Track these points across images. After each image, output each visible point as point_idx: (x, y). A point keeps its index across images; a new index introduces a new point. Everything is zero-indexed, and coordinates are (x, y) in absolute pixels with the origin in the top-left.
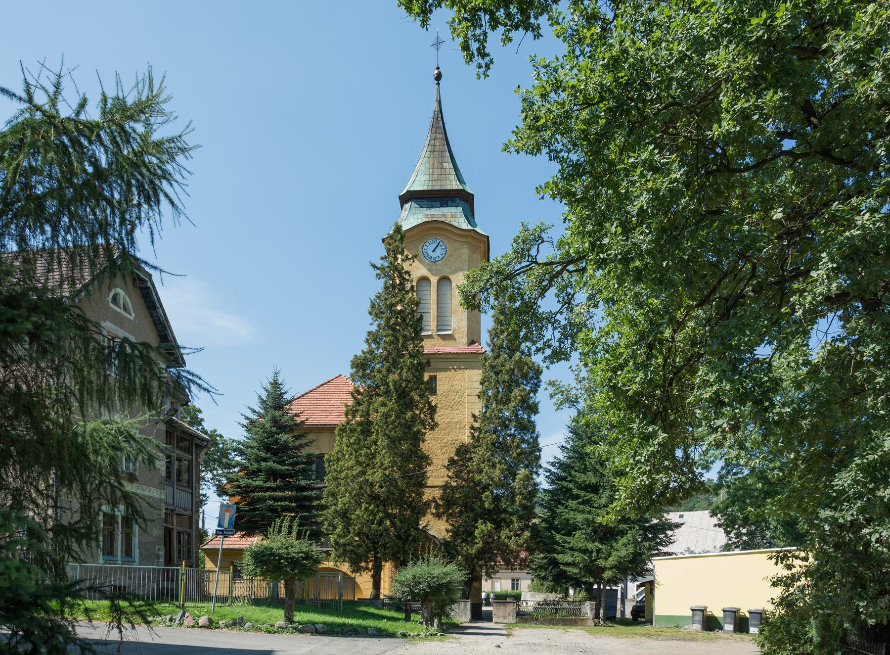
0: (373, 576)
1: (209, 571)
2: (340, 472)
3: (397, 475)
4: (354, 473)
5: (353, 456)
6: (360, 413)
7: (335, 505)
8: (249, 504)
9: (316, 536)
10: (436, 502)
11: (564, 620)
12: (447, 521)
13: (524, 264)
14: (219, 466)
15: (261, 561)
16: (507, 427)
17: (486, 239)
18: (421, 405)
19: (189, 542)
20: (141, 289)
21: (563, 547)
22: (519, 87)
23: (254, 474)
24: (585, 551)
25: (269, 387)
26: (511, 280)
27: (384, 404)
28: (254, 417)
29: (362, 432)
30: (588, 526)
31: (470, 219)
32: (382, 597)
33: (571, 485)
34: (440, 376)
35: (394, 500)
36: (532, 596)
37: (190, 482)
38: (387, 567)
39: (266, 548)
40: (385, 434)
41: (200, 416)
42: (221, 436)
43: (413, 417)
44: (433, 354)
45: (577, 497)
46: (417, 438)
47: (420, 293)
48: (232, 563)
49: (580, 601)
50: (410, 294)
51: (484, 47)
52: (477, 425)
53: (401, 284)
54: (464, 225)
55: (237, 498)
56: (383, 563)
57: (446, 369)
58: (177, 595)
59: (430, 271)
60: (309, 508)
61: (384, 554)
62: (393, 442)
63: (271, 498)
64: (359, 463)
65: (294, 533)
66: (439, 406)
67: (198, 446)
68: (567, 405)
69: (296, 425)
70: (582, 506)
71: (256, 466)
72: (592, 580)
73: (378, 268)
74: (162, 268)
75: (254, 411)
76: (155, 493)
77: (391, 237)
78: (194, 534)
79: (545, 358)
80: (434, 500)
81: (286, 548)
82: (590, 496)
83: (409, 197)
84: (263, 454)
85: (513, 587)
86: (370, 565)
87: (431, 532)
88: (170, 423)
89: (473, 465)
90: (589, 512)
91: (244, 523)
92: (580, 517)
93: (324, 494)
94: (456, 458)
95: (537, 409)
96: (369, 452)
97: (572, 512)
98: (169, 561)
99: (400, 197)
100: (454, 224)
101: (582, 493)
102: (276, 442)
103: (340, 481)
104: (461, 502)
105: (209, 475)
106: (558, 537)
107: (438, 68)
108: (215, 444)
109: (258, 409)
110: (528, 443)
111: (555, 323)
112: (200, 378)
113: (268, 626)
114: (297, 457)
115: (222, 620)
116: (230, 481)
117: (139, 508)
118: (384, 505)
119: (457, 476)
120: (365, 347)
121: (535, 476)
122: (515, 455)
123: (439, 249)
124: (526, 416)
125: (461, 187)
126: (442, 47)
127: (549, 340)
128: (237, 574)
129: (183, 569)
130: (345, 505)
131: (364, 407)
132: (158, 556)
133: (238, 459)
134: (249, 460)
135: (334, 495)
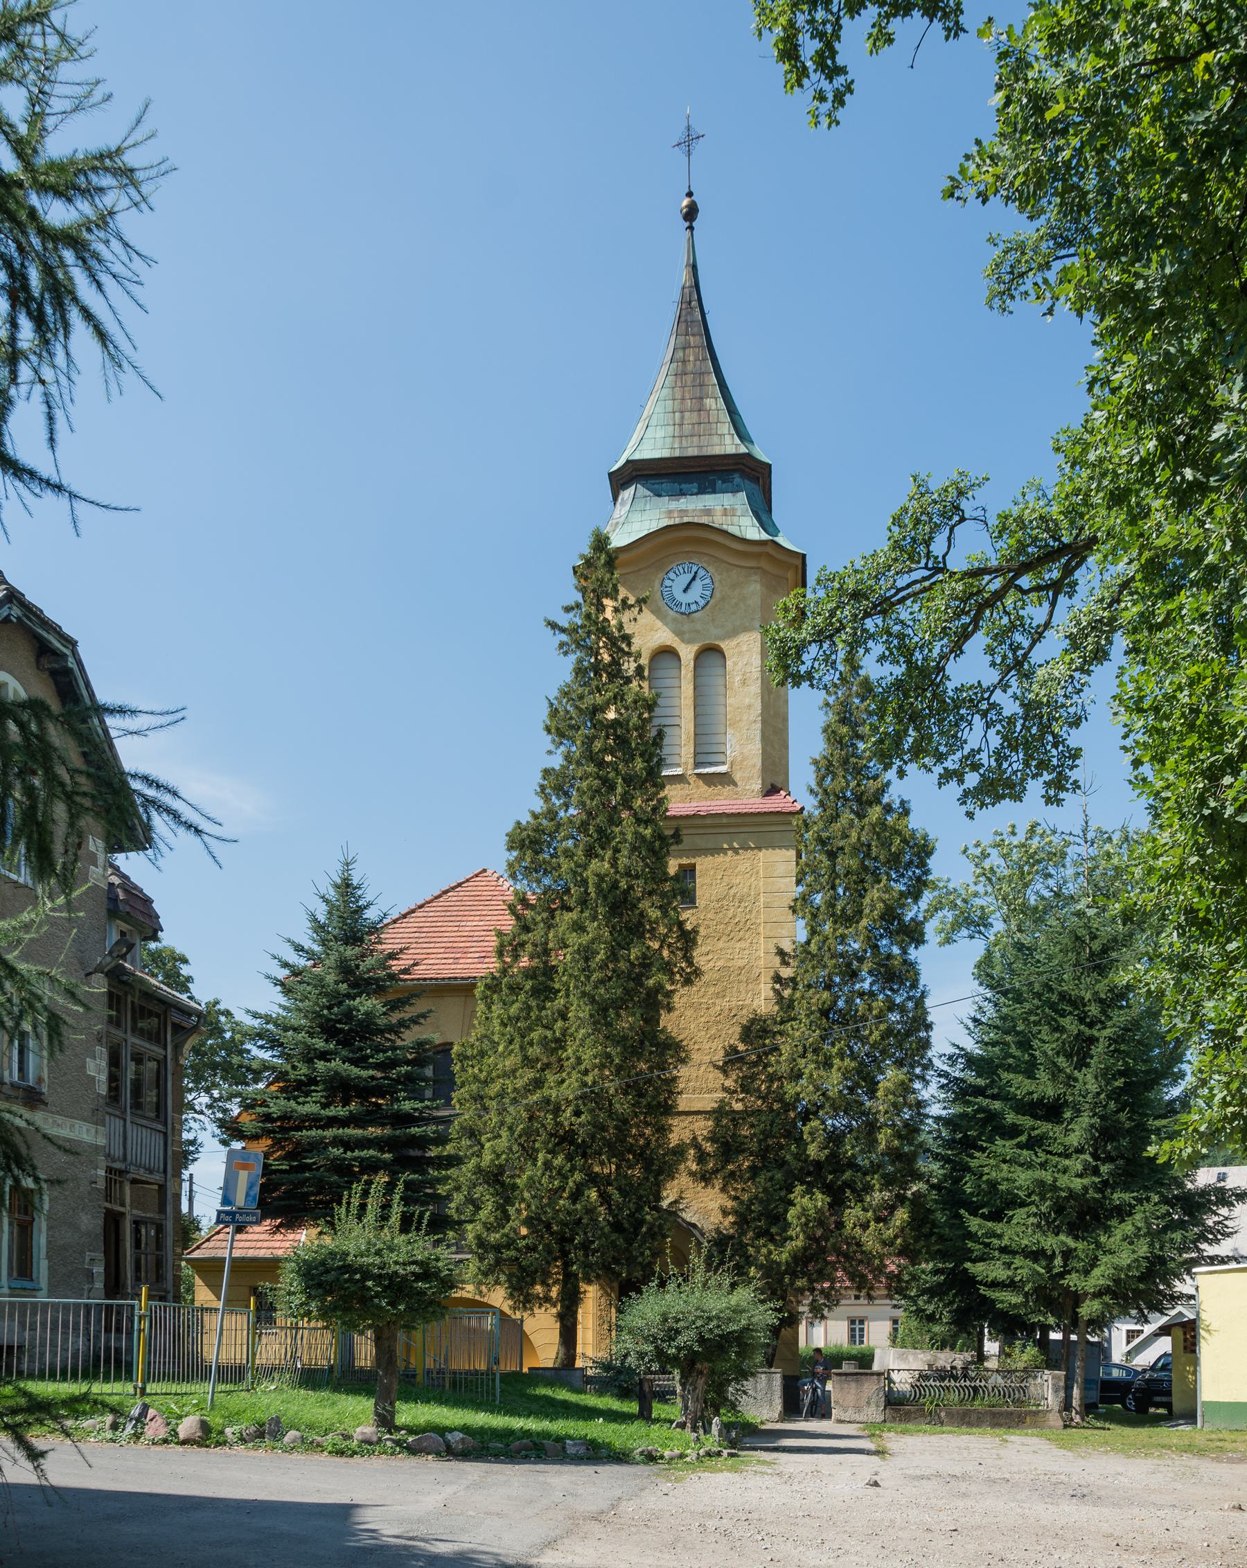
0: (561, 1317)
1: (203, 1310)
2: (486, 1083)
3: (611, 1087)
4: (519, 1083)
5: (516, 1046)
6: (529, 947)
7: (479, 1155)
8: (289, 1156)
9: (440, 1224)
10: (697, 1147)
11: (994, 1415)
12: (723, 1190)
13: (917, 575)
14: (224, 1079)
15: (320, 1285)
16: (854, 975)
17: (799, 562)
18: (663, 930)
19: (159, 1243)
20: (53, 674)
21: (987, 1245)
22: (990, 19)
23: (300, 1088)
24: (1036, 1255)
25: (332, 894)
26: (884, 612)
27: (578, 927)
28: (302, 962)
29: (535, 992)
30: (1043, 1199)
31: (764, 518)
32: (579, 1363)
33: (997, 1105)
34: (704, 864)
35: (608, 1144)
36: (901, 1357)
37: (160, 1108)
38: (592, 1295)
39: (332, 1254)
40: (584, 994)
41: (185, 970)
42: (228, 1013)
43: (644, 956)
44: (688, 817)
45: (1013, 1132)
46: (655, 1003)
47: (657, 683)
48: (254, 1291)
49: (1025, 1370)
50: (634, 684)
51: (833, 53)
52: (786, 973)
53: (615, 663)
54: (753, 532)
55: (266, 1143)
56: (583, 1286)
57: (717, 850)
58: (129, 1365)
59: (679, 633)
60: (420, 1164)
61: (586, 1266)
62: (602, 1012)
63: (338, 1141)
64: (528, 1062)
65: (395, 1219)
66: (702, 931)
67: (177, 1028)
68: (964, 932)
69: (392, 977)
70: (1025, 1152)
71: (304, 1069)
72: (1051, 1320)
73: (563, 630)
74: (74, 488)
75: (299, 948)
76: (83, 1133)
77: (589, 563)
78: (169, 1226)
79: (966, 793)
80: (695, 1143)
81: (378, 1253)
82: (1044, 1127)
83: (623, 478)
84: (319, 1044)
85: (852, 1337)
86: (554, 1292)
87: (688, 1216)
88: (117, 976)
89: (780, 1063)
90: (1043, 1165)
91: (279, 1198)
92: (1024, 1178)
93: (454, 1130)
94: (741, 1047)
95: (922, 934)
96: (549, 1034)
97: (1005, 1167)
98: (114, 1286)
99: (610, 475)
100: (732, 530)
101: (1026, 1121)
102: (348, 1015)
103: (488, 1102)
104: (754, 1146)
105: (204, 1099)
106: (974, 1224)
107: (690, 194)
108: (217, 1031)
109: (307, 944)
110: (902, 1009)
111: (990, 713)
112: (175, 794)
113: (338, 1439)
114: (394, 1049)
115: (231, 1424)
116: (247, 1107)
117: (24, 1151)
118: (584, 1155)
119: (745, 1089)
120: (538, 805)
121: (917, 1085)
122: (876, 1035)
123: (698, 584)
124: (896, 950)
125: (743, 450)
126: (698, 147)
127: (974, 752)
128: (265, 1314)
129: (142, 1304)
130: (498, 1156)
131: (536, 935)
132: (90, 1276)
133: (265, 1055)
134: (288, 1058)
135: (472, 1133)
